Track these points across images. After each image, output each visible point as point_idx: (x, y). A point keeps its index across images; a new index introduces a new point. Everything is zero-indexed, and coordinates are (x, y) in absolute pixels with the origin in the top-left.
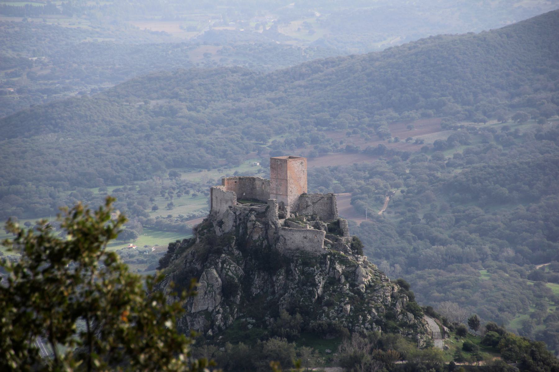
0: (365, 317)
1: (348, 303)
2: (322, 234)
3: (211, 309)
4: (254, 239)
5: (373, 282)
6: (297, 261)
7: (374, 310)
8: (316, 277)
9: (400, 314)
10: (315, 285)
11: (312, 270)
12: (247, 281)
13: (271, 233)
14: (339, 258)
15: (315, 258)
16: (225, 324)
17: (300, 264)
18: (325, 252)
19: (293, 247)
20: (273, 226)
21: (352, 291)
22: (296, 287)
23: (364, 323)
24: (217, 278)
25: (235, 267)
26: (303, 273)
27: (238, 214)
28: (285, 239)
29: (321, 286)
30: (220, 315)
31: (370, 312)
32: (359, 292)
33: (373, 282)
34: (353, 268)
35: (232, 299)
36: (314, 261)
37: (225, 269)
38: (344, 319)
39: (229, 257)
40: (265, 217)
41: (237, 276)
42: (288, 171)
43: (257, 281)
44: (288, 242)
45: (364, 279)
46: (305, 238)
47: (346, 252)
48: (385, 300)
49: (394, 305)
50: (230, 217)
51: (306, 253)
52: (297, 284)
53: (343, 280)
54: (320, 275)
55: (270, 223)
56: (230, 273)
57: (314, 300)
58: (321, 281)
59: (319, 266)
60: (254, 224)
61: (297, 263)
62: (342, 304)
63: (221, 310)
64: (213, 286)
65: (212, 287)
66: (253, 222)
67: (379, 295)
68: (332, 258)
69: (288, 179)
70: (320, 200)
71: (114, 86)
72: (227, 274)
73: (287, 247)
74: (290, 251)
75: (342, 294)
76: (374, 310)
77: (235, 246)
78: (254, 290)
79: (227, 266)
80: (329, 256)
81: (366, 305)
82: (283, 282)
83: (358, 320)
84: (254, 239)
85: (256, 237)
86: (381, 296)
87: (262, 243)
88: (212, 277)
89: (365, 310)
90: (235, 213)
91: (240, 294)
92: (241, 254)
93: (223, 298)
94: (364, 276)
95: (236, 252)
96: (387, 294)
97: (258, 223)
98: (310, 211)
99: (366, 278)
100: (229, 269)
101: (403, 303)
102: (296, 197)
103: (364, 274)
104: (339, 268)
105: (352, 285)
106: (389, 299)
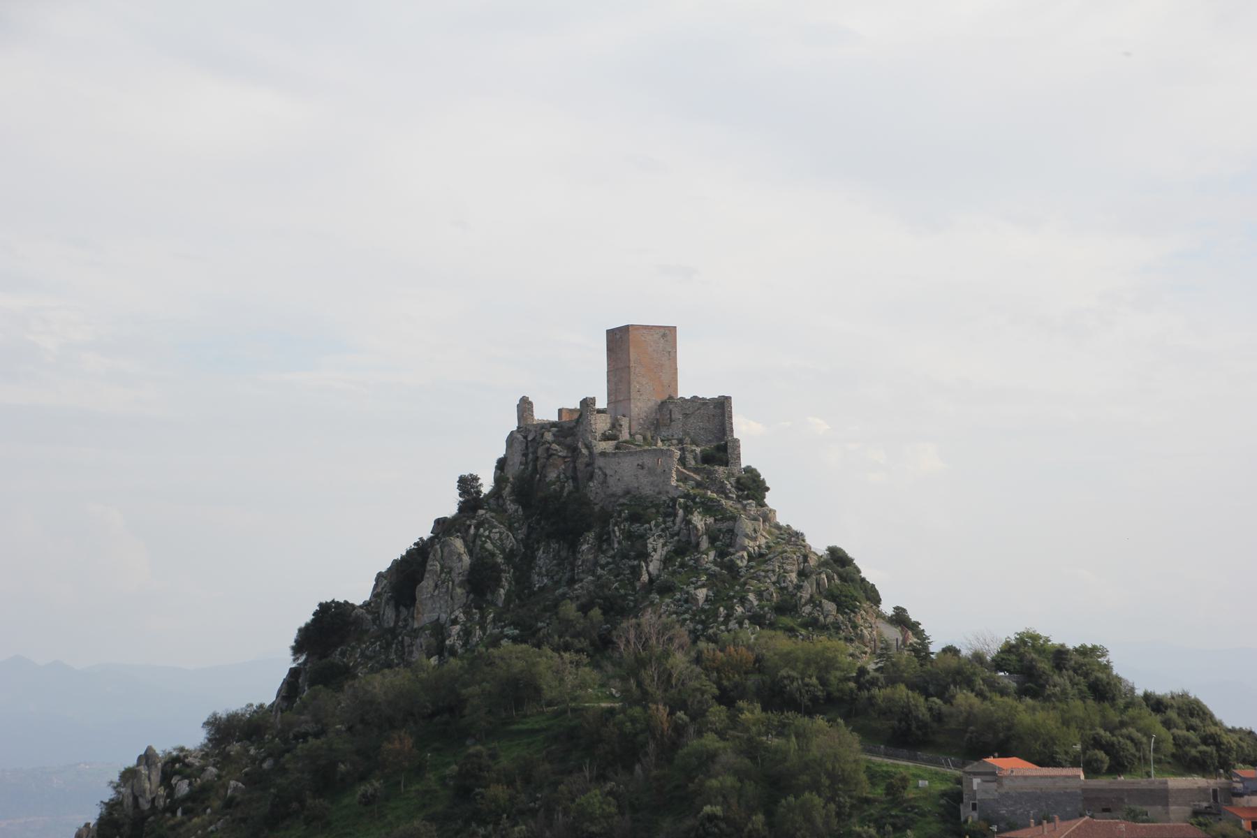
0: (730, 609)
1: (703, 586)
2: (671, 456)
3: (443, 616)
5: (769, 547)
6: (620, 513)
7: (751, 596)
9: (806, 604)
10: (644, 556)
12: (523, 561)
14: (702, 503)
15: (657, 506)
16: (464, 645)
17: (626, 520)
18: (674, 494)
19: (616, 487)
20: (584, 451)
21: (722, 566)
22: (608, 563)
23: (726, 622)
24: (460, 554)
25: (501, 534)
26: (629, 536)
27: (530, 438)
29: (656, 556)
30: (458, 627)
31: (743, 600)
32: (732, 568)
33: (769, 547)
35: (489, 597)
36: (654, 510)
37: (481, 536)
38: (687, 616)
41: (503, 551)
42: (632, 350)
43: (543, 558)
44: (611, 481)
45: (746, 542)
46: (642, 467)
48: (782, 577)
49: (799, 587)
52: (613, 557)
53: (705, 544)
54: (660, 536)
55: (580, 445)
56: (489, 546)
57: (638, 585)
58: (658, 549)
60: (548, 449)
61: (620, 516)
62: (691, 589)
63: (462, 617)
64: (451, 570)
65: (450, 572)
67: (770, 567)
69: (632, 364)
71: (990, 760)
72: (482, 547)
73: (609, 492)
75: (696, 570)
76: (751, 596)
78: (536, 578)
81: (737, 588)
82: (590, 557)
83: (717, 615)
85: (552, 475)
86: (773, 571)
87: (562, 488)
88: (451, 553)
89: (734, 597)
90: (525, 437)
91: (507, 587)
92: (520, 511)
93: (472, 596)
94: (747, 536)
95: (511, 507)
96: (789, 568)
97: (555, 446)
98: (677, 430)
99: (755, 539)
100: (488, 537)
101: (818, 584)
102: (651, 404)
103: (749, 531)
104: (698, 520)
105: (722, 554)
106: (794, 576)
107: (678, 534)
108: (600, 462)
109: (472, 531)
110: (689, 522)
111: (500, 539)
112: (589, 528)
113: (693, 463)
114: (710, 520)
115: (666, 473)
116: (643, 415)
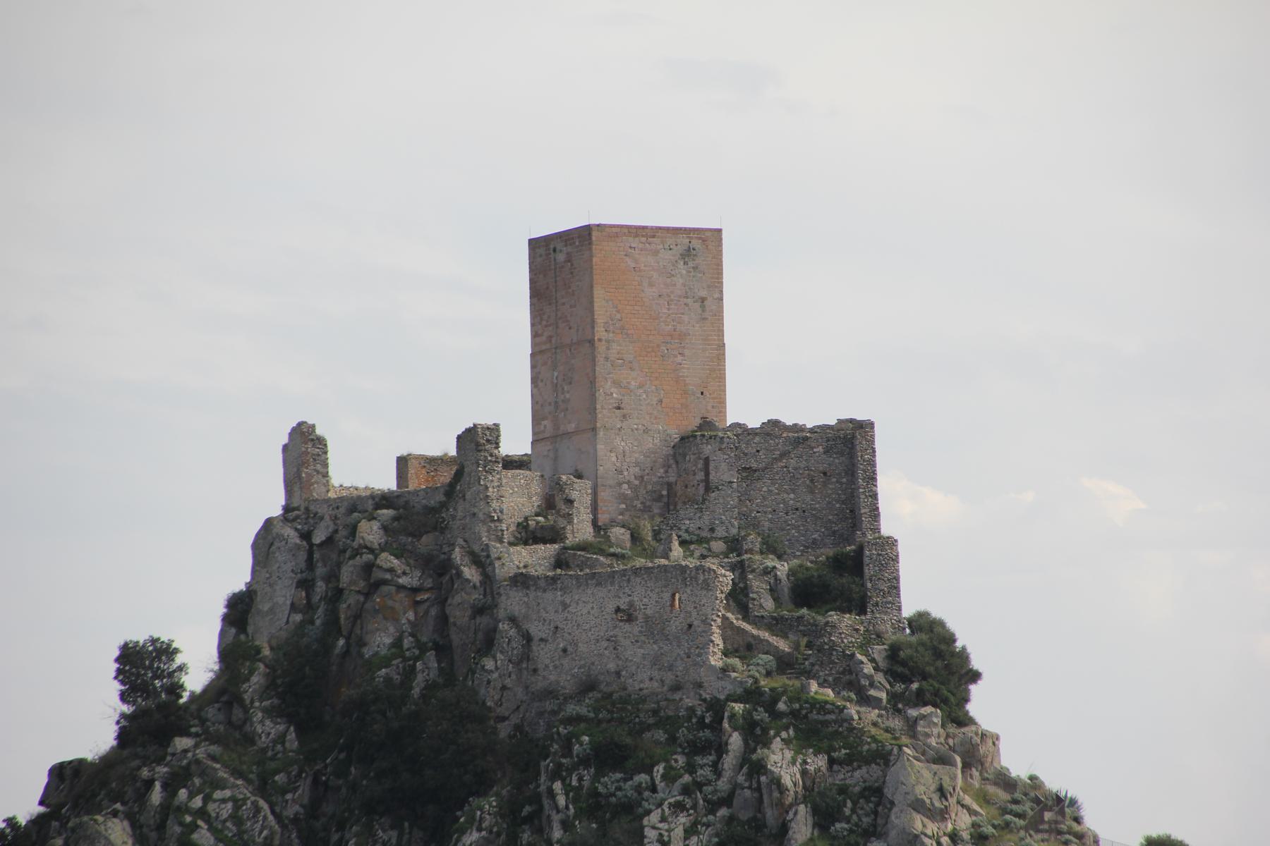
4: (367, 652)
8: (654, 817)
11: (638, 789)
13: (460, 604)
14: (794, 714)
17: (584, 762)
19: (563, 677)
20: (470, 573)
25: (237, 803)
28: (528, 638)
34: (875, 770)
36: (661, 735)
39: (214, 749)
40: (440, 528)
42: (598, 293)
44: (544, 655)
47: (850, 681)
50: (280, 557)
51: (625, 701)
54: (679, 807)
55: (457, 555)
59: (681, 760)
60: (369, 568)
66: (368, 557)
68: (761, 715)
69: (600, 332)
70: (784, 455)
73: (539, 684)
74: (549, 705)
77: (265, 692)
79: (191, 796)
80: (738, 707)
84: (367, 652)
85: (381, 640)
87: (410, 673)
90: (306, 536)
94: (918, 806)
95: (266, 728)
98: (723, 513)
99: (941, 815)
102: (652, 442)
104: (784, 763)
107: (727, 801)
108: (512, 602)
109: (156, 796)
110: (758, 768)
111: (236, 818)
112: (482, 786)
113: (769, 604)
114: (817, 763)
115: (694, 632)
116: (630, 473)
